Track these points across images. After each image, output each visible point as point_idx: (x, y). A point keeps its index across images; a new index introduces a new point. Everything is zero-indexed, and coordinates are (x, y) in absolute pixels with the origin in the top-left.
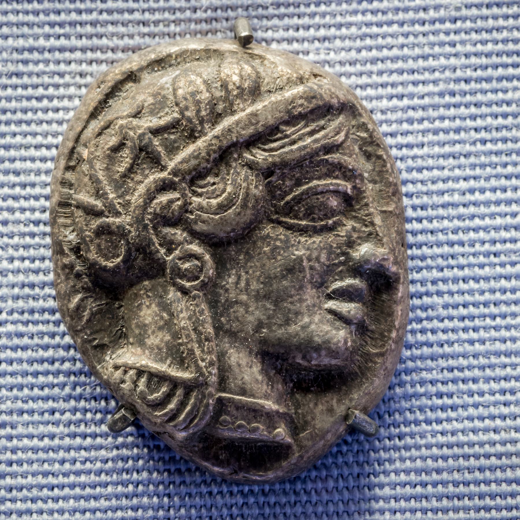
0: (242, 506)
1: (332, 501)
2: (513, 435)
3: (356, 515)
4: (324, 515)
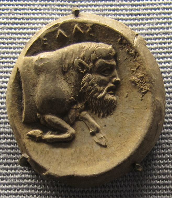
0: (125, 191)
1: (140, 190)
2: (169, 59)
3: (137, 196)
4: (111, 196)
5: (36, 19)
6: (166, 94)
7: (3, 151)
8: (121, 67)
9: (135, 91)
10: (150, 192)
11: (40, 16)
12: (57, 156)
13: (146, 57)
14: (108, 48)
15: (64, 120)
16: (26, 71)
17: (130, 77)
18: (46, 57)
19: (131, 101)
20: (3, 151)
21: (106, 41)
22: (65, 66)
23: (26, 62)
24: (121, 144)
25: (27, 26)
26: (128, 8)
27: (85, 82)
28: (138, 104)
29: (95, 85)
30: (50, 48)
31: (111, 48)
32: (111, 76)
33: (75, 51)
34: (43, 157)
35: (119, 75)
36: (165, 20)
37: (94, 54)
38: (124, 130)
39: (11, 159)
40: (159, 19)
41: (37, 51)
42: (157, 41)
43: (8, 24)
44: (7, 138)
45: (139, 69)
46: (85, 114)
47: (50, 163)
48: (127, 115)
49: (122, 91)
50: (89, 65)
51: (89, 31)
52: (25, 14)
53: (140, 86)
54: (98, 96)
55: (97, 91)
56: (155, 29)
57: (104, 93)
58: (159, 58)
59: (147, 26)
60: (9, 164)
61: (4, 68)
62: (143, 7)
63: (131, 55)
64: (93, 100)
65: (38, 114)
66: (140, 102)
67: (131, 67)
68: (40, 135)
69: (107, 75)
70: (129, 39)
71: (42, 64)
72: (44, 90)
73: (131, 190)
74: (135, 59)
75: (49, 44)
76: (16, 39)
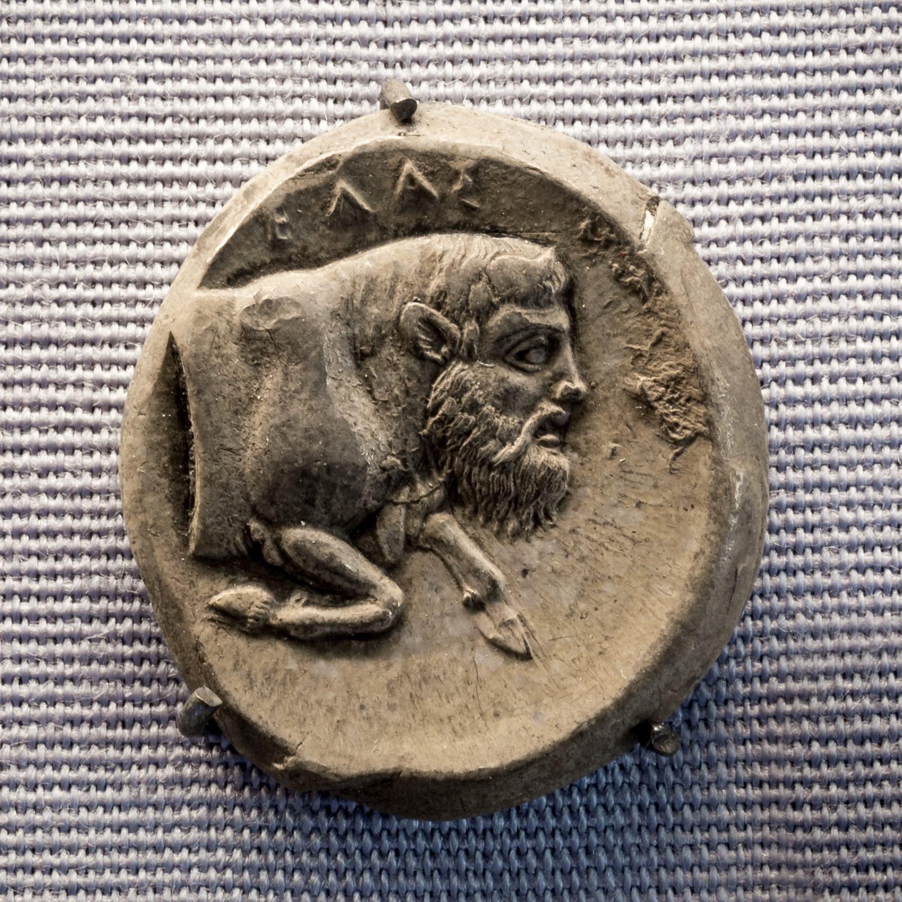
1: (665, 826)
5: (229, 118)
6: (769, 429)
7: (103, 669)
8: (591, 335)
9: (647, 434)
10: (706, 835)
11: (246, 105)
12: (331, 695)
13: (692, 295)
14: (540, 260)
15: (360, 550)
16: (206, 347)
17: (626, 375)
18: (289, 296)
19: (631, 472)
20: (103, 669)
21: (528, 228)
22: (362, 330)
23: (207, 312)
24: (589, 647)
25: (193, 148)
26: (611, 71)
27: (446, 397)
28: (655, 486)
29: (485, 409)
30: (303, 256)
31: (550, 261)
32: (548, 374)
33: (404, 273)
34: (274, 698)
35: (584, 367)
36: (767, 121)
37: (480, 285)
38: (600, 591)
39: (138, 702)
40: (740, 115)
41: (247, 267)
42: (733, 209)
43: (114, 141)
44: (121, 617)
45: (662, 345)
46: (443, 525)
47: (302, 722)
48: (615, 531)
49: (591, 434)
50: (461, 329)
51: (461, 190)
52: (184, 96)
53: (667, 415)
54: (496, 453)
55: (491, 432)
56: (724, 158)
57: (519, 442)
58: (740, 281)
59: (689, 147)
60: (126, 723)
61: (98, 324)
62: (672, 66)
63: (635, 290)
64: (476, 470)
65: (254, 525)
66: (665, 480)
67: (632, 336)
68: (262, 608)
69: (537, 367)
70: (624, 226)
71: (270, 324)
72: (281, 430)
73: (630, 825)
74: (645, 307)
75: (298, 238)
76: (145, 204)
